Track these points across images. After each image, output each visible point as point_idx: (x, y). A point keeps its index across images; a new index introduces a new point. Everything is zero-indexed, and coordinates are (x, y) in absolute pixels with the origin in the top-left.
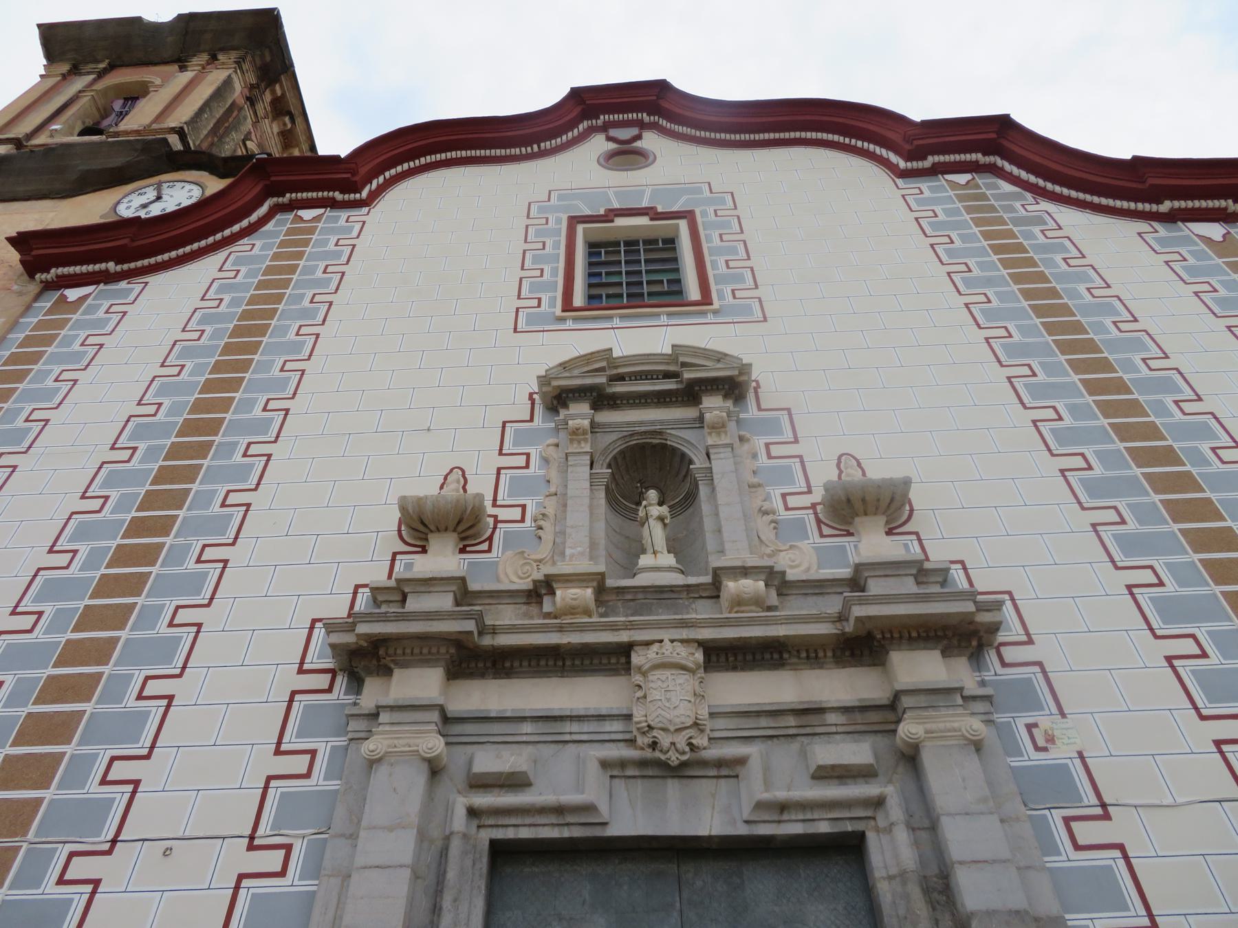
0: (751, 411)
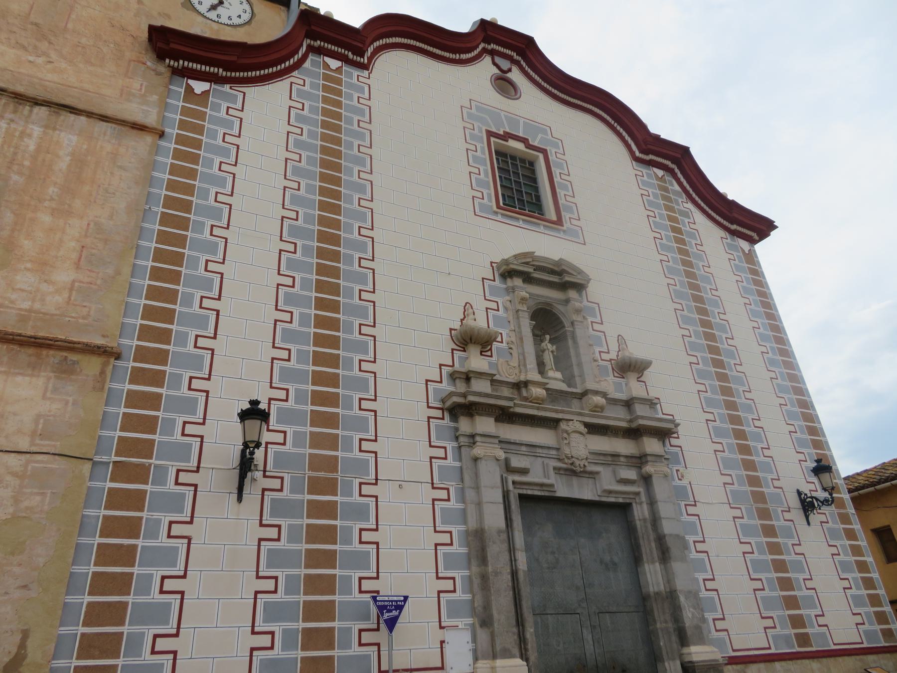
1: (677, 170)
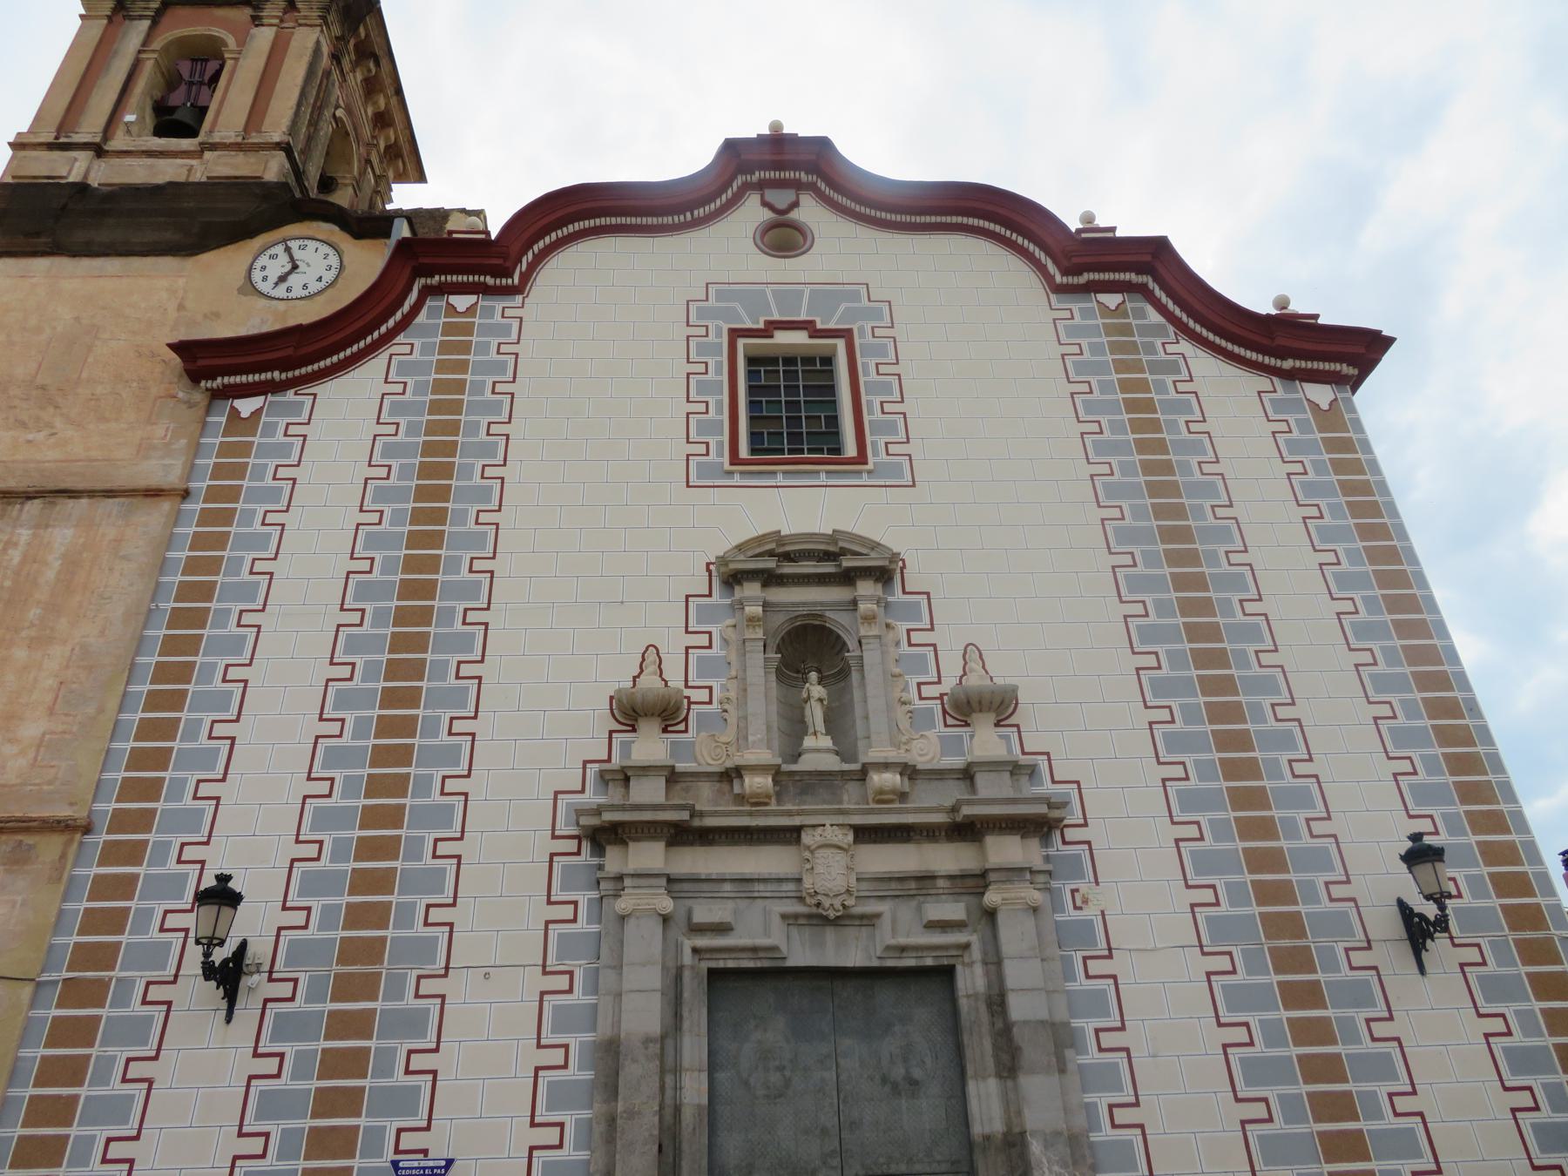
0: (897, 596)
1: (1152, 285)
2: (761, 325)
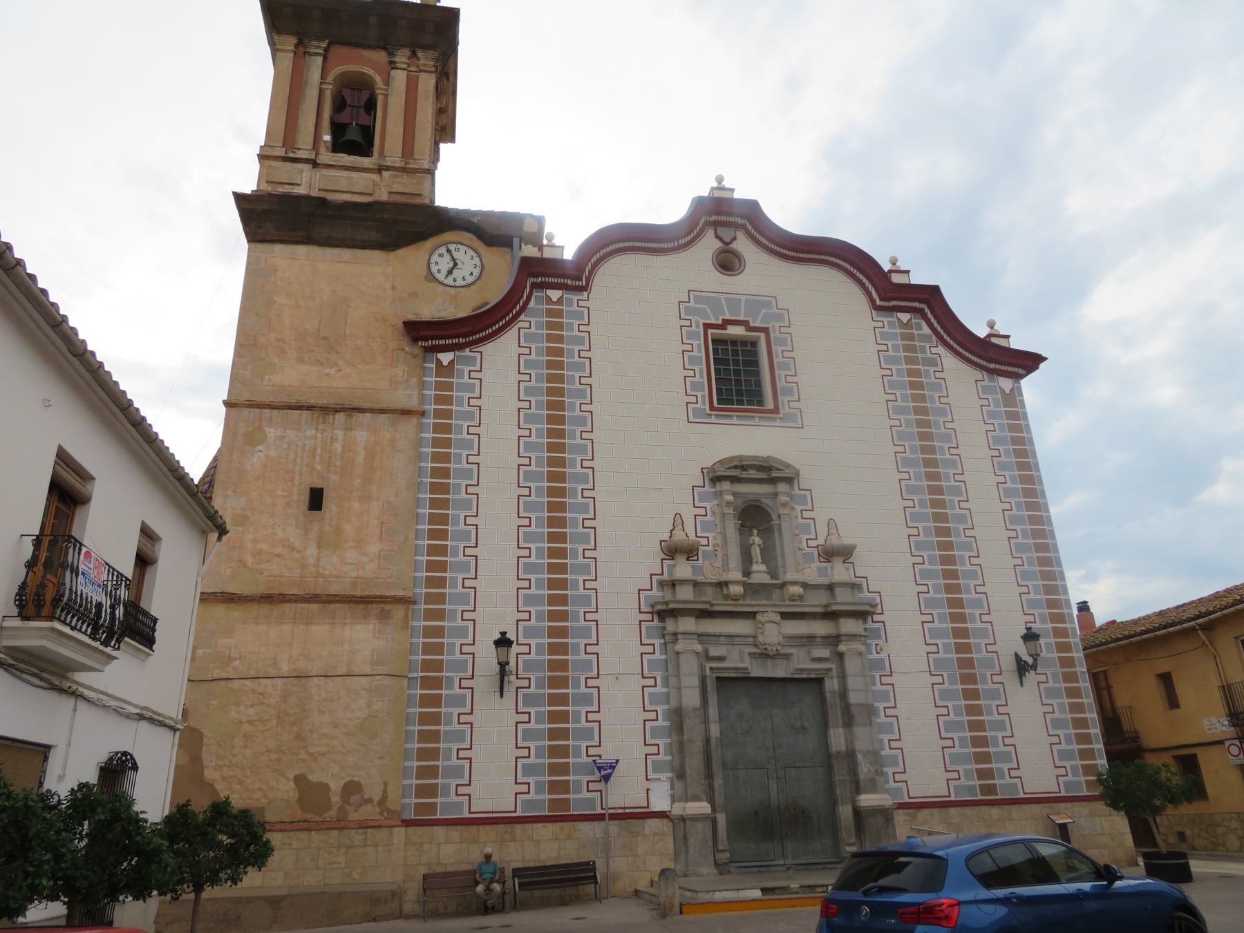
2: (720, 322)
